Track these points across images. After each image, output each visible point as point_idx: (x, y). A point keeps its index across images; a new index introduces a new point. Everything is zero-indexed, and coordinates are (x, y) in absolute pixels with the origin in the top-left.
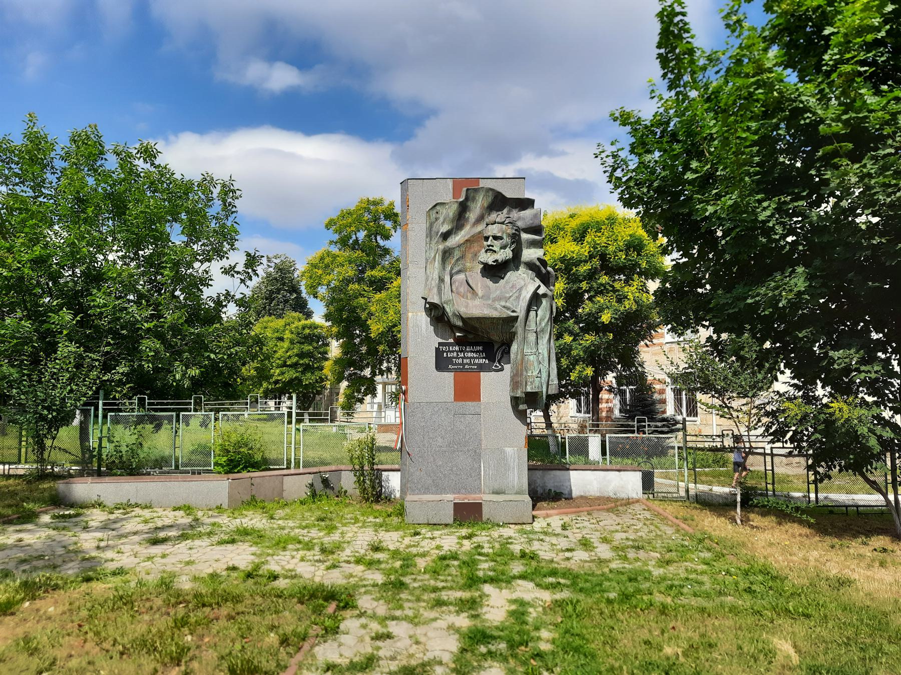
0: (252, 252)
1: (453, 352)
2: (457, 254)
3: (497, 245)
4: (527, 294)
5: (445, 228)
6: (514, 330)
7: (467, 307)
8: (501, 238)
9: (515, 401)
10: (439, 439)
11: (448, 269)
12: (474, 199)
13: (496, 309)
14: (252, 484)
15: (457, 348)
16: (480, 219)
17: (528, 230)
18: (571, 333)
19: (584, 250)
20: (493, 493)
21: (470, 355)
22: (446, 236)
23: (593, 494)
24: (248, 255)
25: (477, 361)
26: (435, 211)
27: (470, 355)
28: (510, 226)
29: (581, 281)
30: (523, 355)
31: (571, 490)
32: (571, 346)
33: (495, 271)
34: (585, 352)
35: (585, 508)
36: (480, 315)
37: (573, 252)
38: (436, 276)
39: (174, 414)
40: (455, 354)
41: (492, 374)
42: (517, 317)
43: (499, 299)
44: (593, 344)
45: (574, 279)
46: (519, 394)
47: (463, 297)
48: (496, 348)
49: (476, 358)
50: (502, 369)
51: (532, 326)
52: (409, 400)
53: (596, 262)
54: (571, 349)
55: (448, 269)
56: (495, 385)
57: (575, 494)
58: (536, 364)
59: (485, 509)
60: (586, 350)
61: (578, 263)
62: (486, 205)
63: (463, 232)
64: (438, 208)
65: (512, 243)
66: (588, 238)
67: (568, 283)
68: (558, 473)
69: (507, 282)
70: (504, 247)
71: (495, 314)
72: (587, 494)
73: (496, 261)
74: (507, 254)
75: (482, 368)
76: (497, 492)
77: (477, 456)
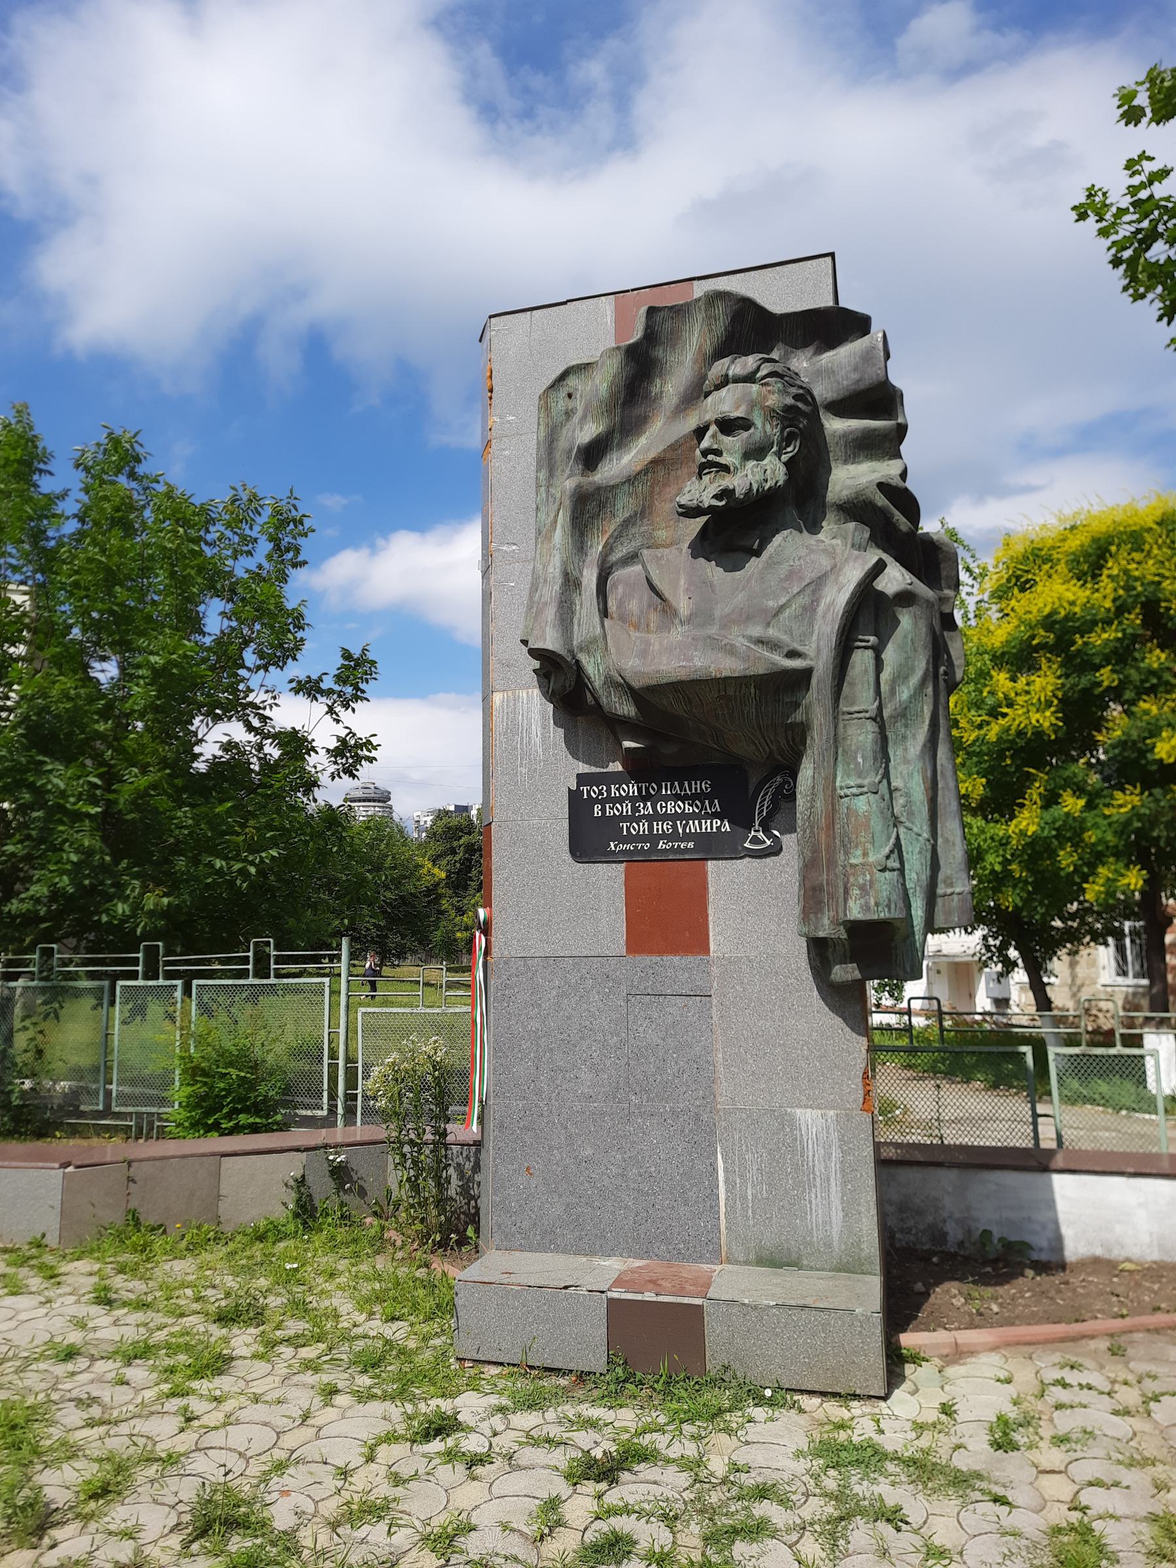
0: (356, 652)
1: (621, 800)
2: (624, 507)
3: (732, 447)
4: (838, 597)
5: (588, 432)
6: (799, 716)
7: (644, 654)
8: (744, 424)
9: (821, 952)
10: (585, 1075)
11: (596, 548)
12: (674, 339)
13: (731, 650)
14: (131, 1180)
15: (633, 789)
16: (697, 392)
17: (842, 407)
18: (1079, 790)
19: (1104, 595)
20: (761, 1262)
21: (671, 807)
22: (592, 455)
23: (1135, 1252)
24: (347, 655)
25: (693, 826)
26: (563, 393)
27: (671, 807)
28: (776, 384)
29: (1097, 668)
30: (834, 798)
31: (1059, 1239)
32: (1083, 820)
33: (733, 531)
34: (1119, 834)
35: (1104, 1324)
36: (683, 675)
37: (1073, 603)
38: (554, 570)
39: (106, 983)
40: (627, 809)
41: (744, 865)
42: (807, 673)
43: (746, 617)
44: (1135, 813)
45: (1077, 663)
46: (826, 928)
47: (637, 627)
48: (753, 781)
49: (693, 816)
50: (776, 850)
51: (861, 697)
52: (495, 951)
53: (1134, 619)
54: (1083, 830)
55: (596, 548)
56: (752, 904)
57: (1075, 1247)
58: (877, 824)
59: (714, 1331)
60: (1123, 828)
61: (1089, 625)
63: (643, 441)
64: (572, 382)
65: (788, 440)
66: (1112, 568)
67: (1067, 676)
68: (1012, 1179)
69: (771, 564)
70: (756, 452)
71: (728, 666)
72: (1116, 1254)
73: (725, 493)
74: (772, 470)
75: (712, 848)
76: (775, 1260)
77: (701, 1133)
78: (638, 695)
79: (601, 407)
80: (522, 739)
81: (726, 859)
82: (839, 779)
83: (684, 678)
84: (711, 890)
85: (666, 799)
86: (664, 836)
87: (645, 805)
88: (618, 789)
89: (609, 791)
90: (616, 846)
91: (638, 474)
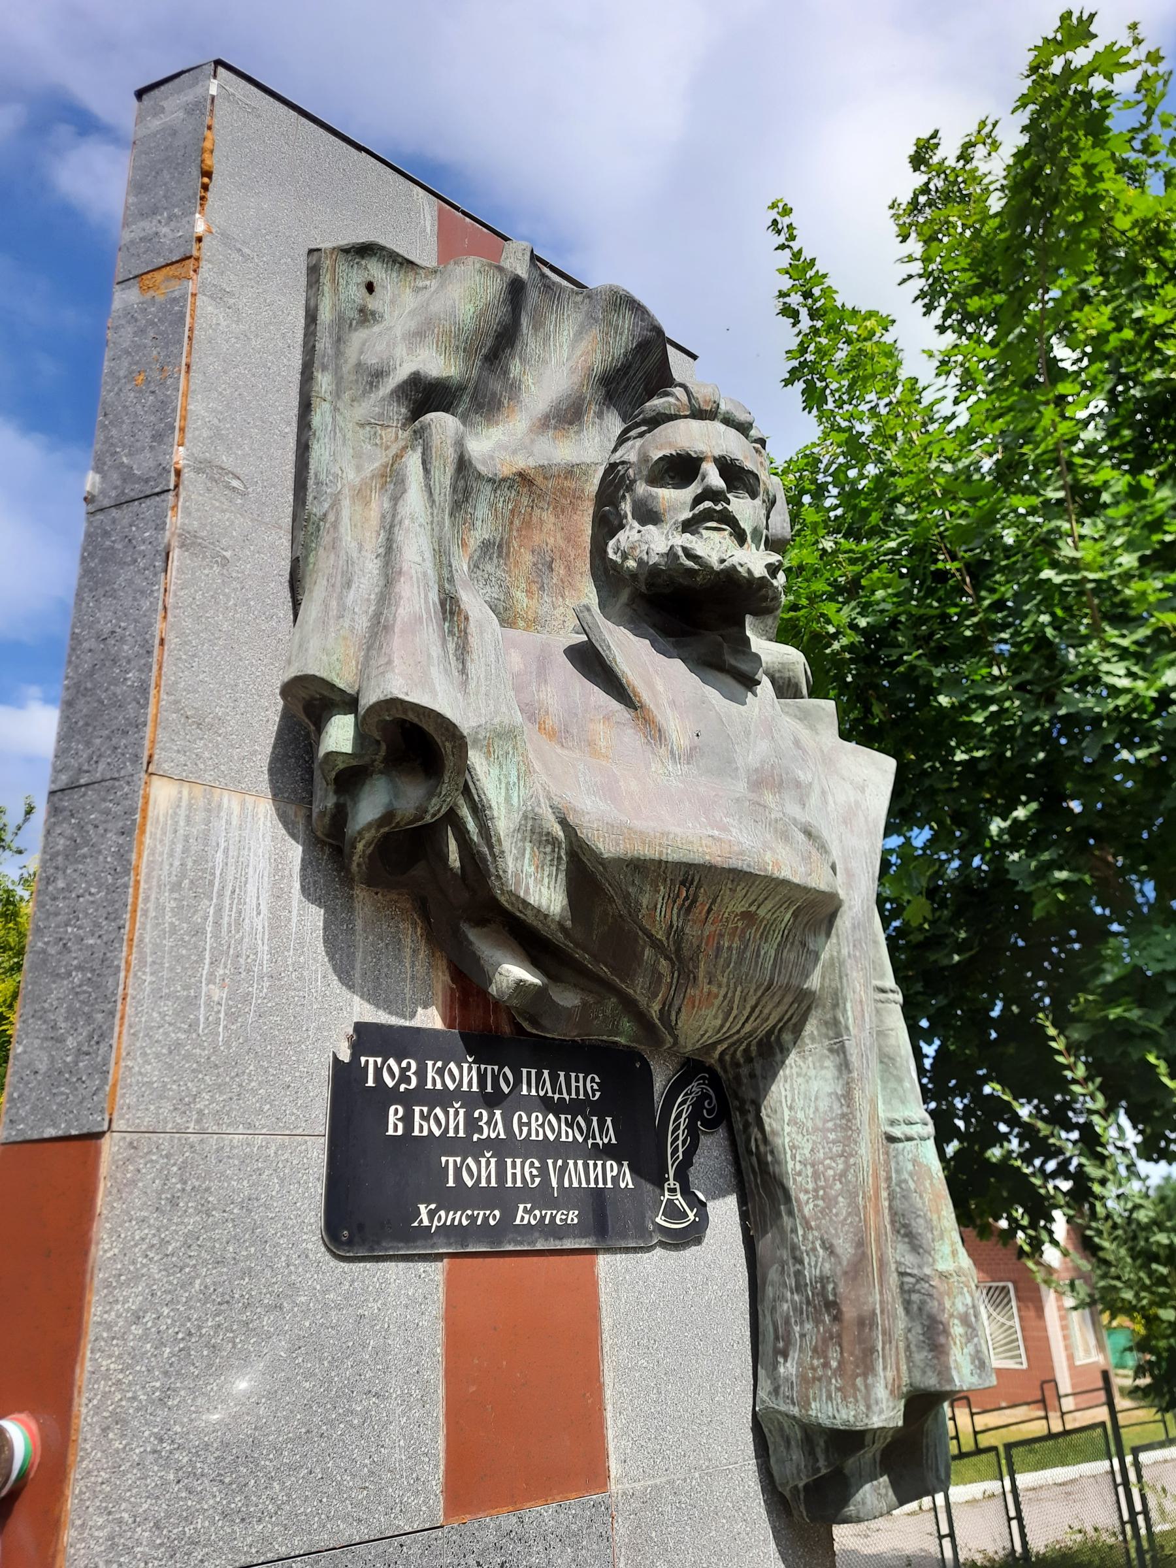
1: (443, 1098)
15: (465, 1075)
40: (454, 1120)
48: (659, 1084)
50: (692, 1236)
62: (598, 368)
64: (375, 270)
75: (604, 1222)
78: (582, 867)
79: (457, 337)
80: (219, 910)
81: (627, 1250)
82: (881, 1106)
83: (718, 861)
84: (606, 1323)
85: (528, 1105)
86: (525, 1194)
87: (491, 1116)
88: (440, 1072)
89: (421, 1074)
90: (432, 1214)
91: (504, 480)
